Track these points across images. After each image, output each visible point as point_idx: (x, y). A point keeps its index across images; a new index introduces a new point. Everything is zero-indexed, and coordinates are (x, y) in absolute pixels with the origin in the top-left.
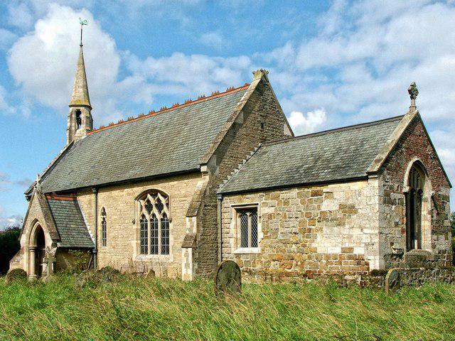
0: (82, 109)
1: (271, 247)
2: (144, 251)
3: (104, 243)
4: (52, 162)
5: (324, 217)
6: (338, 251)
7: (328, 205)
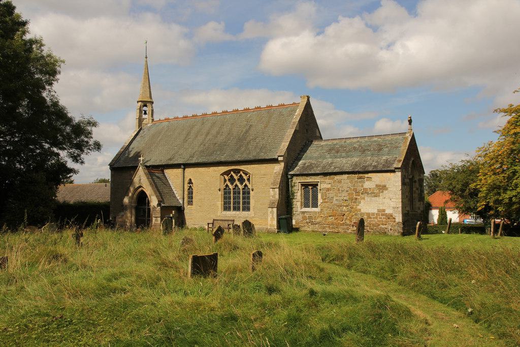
2: (226, 208)
3: (190, 202)
5: (366, 192)
6: (376, 211)
7: (368, 185)
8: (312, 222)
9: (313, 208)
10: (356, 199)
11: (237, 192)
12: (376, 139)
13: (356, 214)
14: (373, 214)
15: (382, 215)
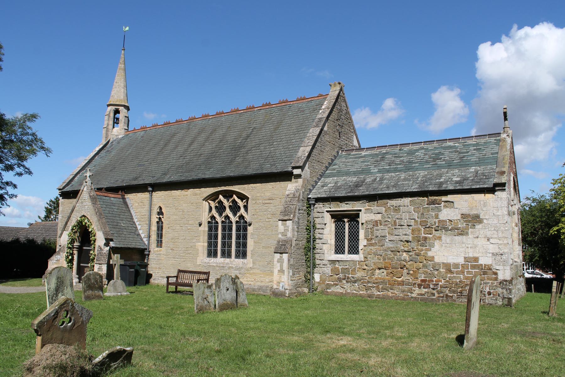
0: (121, 108)
1: (375, 254)
2: (212, 253)
3: (160, 243)
4: (371, 147)
5: (443, 227)
6: (461, 261)
7: (446, 214)
8: (348, 278)
9: (350, 255)
10: (426, 238)
11: (227, 227)
12: (451, 144)
13: (424, 266)
14: (456, 265)
15: (473, 267)
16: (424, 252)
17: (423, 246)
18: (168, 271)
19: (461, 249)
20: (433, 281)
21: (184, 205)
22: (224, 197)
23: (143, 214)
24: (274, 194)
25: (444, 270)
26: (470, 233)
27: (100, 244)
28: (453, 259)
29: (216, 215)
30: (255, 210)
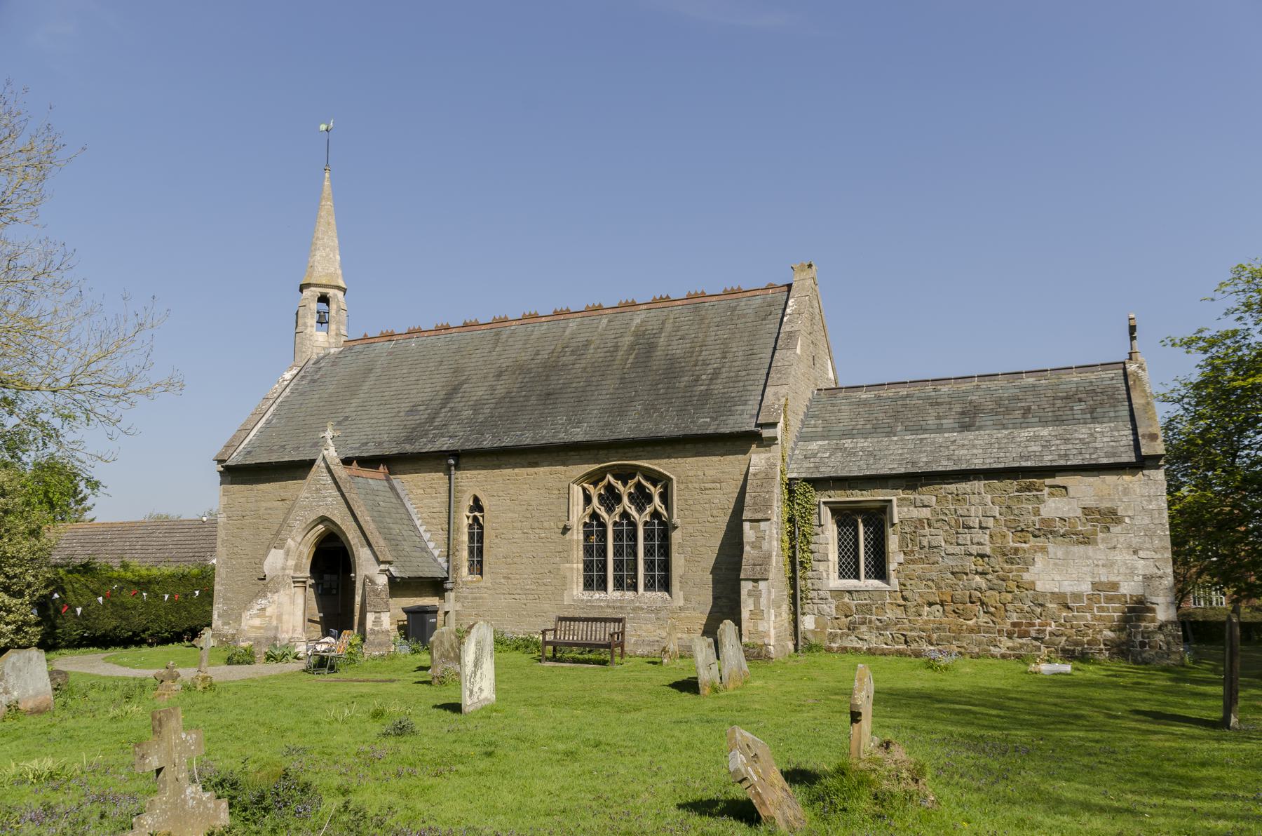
2: (594, 580)
3: (477, 566)
5: (1047, 530)
6: (1086, 588)
7: (1053, 507)
8: (870, 622)
10: (1016, 550)
11: (627, 530)
14: (1077, 597)
15: (1110, 599)
16: (1014, 573)
17: (1012, 563)
18: (497, 621)
19: (1085, 569)
20: (1032, 625)
21: (530, 492)
22: (616, 477)
23: (434, 510)
24: (723, 472)
25: (1055, 606)
26: (1099, 541)
27: (367, 573)
28: (1071, 585)
29: (602, 512)
30: (686, 500)
